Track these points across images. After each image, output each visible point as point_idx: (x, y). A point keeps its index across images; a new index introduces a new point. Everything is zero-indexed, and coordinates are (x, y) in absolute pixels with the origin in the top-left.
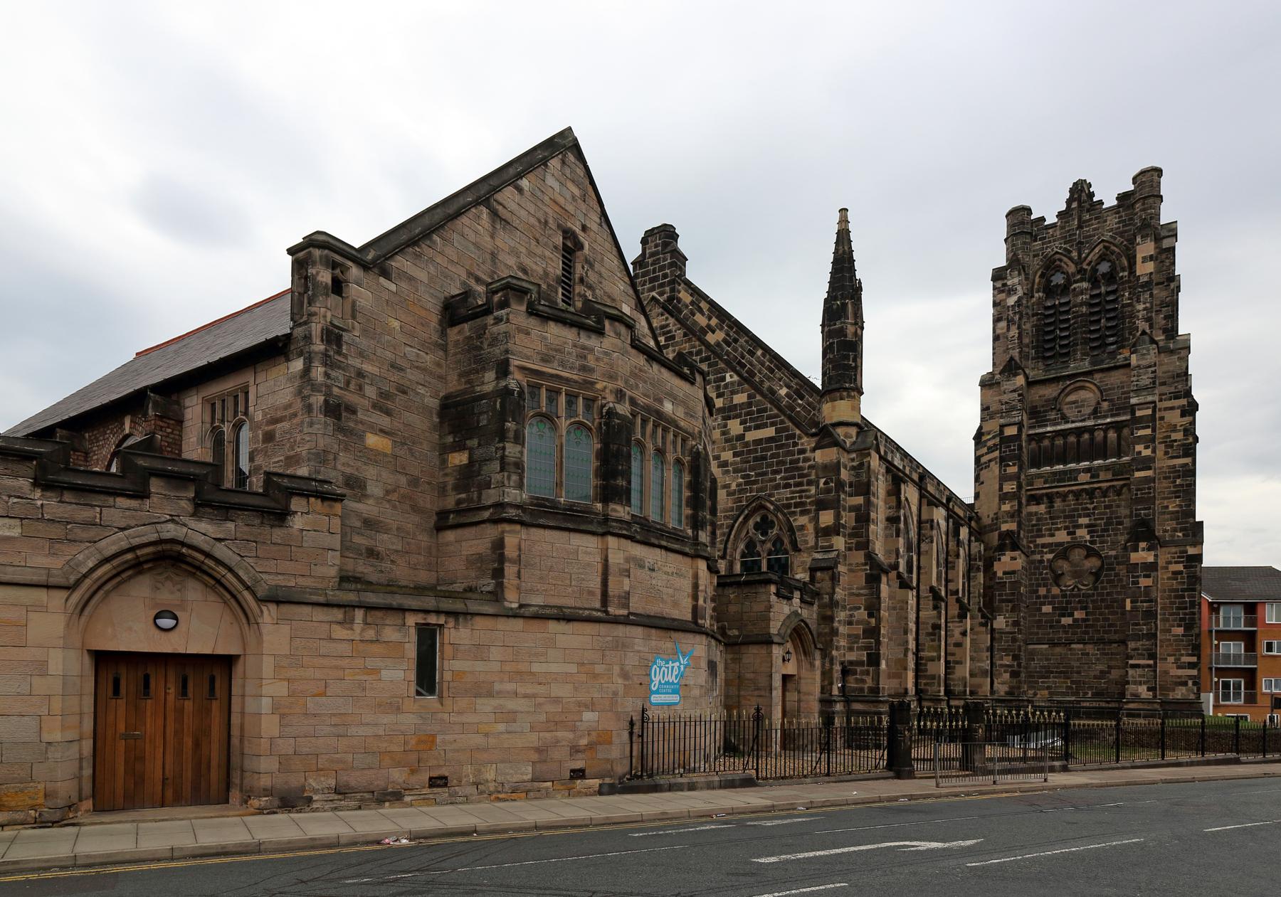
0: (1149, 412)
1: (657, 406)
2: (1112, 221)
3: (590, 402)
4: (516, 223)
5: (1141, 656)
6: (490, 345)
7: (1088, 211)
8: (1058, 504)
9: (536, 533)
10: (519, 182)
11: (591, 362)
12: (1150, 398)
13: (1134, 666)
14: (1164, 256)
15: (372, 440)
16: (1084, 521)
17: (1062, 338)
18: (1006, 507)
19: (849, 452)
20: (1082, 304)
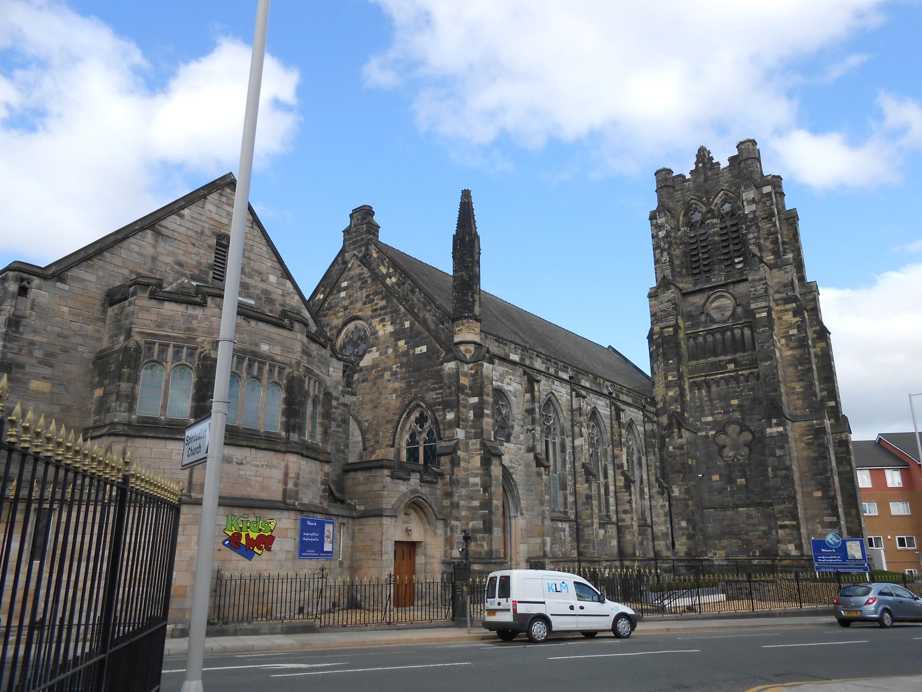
0: (765, 314)
1: (253, 348)
2: (727, 176)
3: (192, 352)
4: (176, 236)
5: (784, 517)
7: (710, 169)
8: (714, 389)
9: (139, 442)
10: (182, 212)
11: (195, 323)
12: (764, 304)
13: (783, 527)
14: (765, 199)
15: (35, 385)
16: (735, 402)
18: (671, 393)
20: (715, 234)
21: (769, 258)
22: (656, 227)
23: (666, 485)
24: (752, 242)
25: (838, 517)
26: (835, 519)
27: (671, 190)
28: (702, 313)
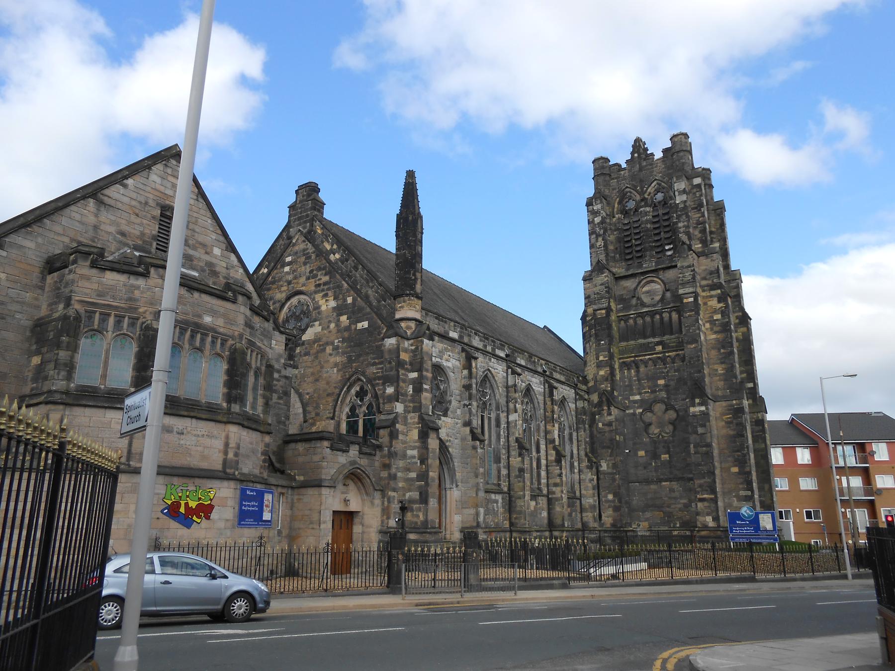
0: (691, 299)
1: (196, 320)
2: (661, 166)
3: (133, 322)
4: (119, 205)
5: (704, 491)
6: (65, 287)
7: (645, 160)
9: (78, 411)
10: (125, 181)
12: (691, 290)
14: (695, 190)
16: (661, 382)
17: (637, 245)
18: (602, 373)
19: (408, 339)
20: (647, 221)
21: (697, 246)
22: (593, 213)
23: (594, 460)
24: (682, 230)
25: (753, 492)
26: (749, 493)
27: (608, 178)
28: (633, 297)
